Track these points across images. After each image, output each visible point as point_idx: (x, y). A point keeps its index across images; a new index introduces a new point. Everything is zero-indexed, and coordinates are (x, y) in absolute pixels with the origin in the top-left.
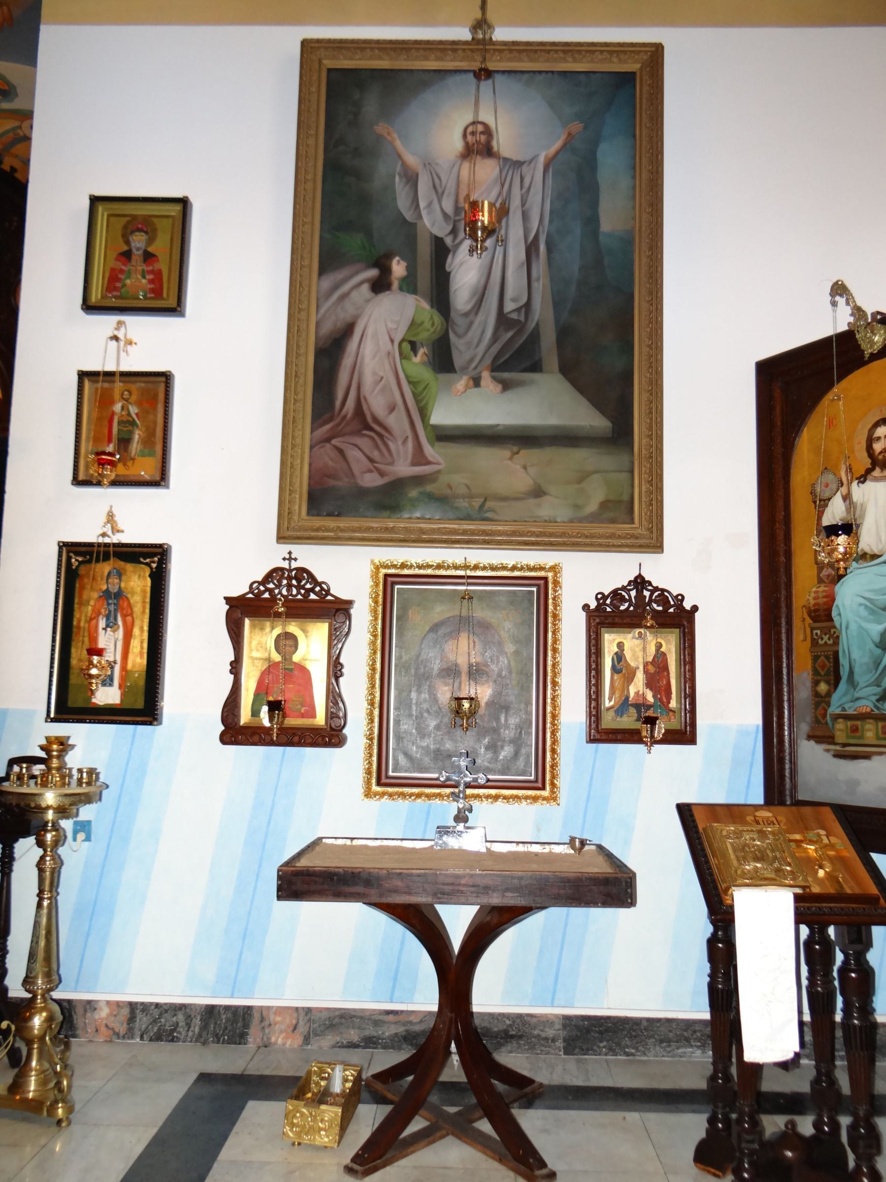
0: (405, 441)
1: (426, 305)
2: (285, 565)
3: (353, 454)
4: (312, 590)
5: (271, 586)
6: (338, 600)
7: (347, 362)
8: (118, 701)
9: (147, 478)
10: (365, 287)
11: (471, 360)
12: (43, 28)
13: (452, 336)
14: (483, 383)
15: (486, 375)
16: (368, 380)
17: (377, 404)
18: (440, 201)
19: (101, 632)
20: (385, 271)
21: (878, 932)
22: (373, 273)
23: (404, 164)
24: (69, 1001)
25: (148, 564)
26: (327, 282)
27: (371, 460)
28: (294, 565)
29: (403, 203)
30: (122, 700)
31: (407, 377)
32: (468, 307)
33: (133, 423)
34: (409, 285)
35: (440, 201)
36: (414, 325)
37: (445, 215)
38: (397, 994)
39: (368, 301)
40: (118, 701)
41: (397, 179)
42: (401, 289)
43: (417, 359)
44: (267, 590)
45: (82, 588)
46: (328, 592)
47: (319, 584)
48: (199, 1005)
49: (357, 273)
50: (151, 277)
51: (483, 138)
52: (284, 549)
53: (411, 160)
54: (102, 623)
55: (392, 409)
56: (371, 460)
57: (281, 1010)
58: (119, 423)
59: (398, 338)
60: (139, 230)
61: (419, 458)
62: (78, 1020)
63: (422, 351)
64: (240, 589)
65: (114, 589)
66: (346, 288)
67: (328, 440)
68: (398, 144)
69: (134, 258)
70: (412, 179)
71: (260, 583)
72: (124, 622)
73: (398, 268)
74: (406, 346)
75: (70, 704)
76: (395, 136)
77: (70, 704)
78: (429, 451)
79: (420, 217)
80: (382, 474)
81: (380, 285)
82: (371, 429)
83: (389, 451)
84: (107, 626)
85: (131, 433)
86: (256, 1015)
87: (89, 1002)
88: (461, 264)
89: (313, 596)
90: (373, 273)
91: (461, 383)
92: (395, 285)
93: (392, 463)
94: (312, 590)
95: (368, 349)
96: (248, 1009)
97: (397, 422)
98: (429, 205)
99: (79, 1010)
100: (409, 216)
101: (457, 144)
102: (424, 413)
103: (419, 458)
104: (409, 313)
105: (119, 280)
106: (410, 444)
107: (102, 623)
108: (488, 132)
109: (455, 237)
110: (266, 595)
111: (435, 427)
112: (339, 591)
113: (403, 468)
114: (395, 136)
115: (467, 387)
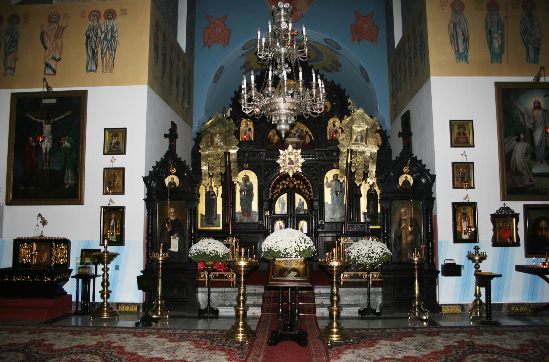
0: (527, 177)
1: (529, 145)
2: (504, 206)
3: (516, 180)
4: (510, 212)
5: (501, 211)
6: (516, 214)
7: (513, 158)
8: (468, 238)
9: (459, 186)
10: (515, 141)
11: (540, 158)
12: (431, 77)
13: (535, 152)
14: (543, 163)
15: (544, 161)
16: (518, 162)
17: (520, 168)
18: (530, 120)
19: (463, 222)
20: (519, 137)
21: (7, 263)
22: (516, 137)
23: (521, 111)
24: (463, 304)
25: (472, 207)
26: (506, 140)
27: (520, 181)
28: (506, 206)
29: (522, 120)
30: (469, 238)
31: (526, 162)
32: (538, 145)
33: (465, 173)
34: (525, 140)
35: (530, 120)
36: (527, 150)
37: (532, 123)
38: (533, 300)
39: (516, 144)
40: (468, 238)
41: (520, 115)
42: (523, 141)
43: (528, 158)
44: (500, 212)
45: (458, 212)
46: (513, 212)
47: (512, 210)
48: (506, 303)
49: (512, 138)
50: (465, 139)
51: (538, 104)
52: (503, 202)
53: (522, 110)
54: (463, 220)
55: (523, 169)
56: (520, 181)
57: (114, 303)
58: (462, 173)
59: (524, 152)
60: (461, 127)
61: (531, 181)
62: (465, 308)
63: (529, 156)
64: (494, 212)
65: (465, 213)
66: (511, 141)
67: (510, 177)
68: (519, 106)
69: (461, 134)
70: (523, 115)
71: (498, 211)
72: (467, 220)
73: (522, 136)
74: (526, 155)
75: (458, 239)
76: (518, 104)
77: (458, 239)
78: (533, 179)
79: (526, 124)
80: (523, 184)
81: (518, 140)
82: (519, 174)
83: (524, 179)
84: (464, 221)
85: (465, 176)
86: (503, 305)
87: (467, 304)
88: (536, 135)
89: (510, 213)
90: (516, 137)
91: (538, 163)
92: (522, 140)
93: (525, 182)
94: (510, 212)
95: (517, 155)
96: (502, 304)
97: (525, 172)
98: (528, 121)
99: (465, 306)
100: (523, 123)
101: (533, 106)
102: (531, 170)
103: (531, 181)
104: (526, 146)
105: (458, 140)
106: (528, 177)
107: (463, 220)
108: (539, 103)
109: (534, 129)
110: (500, 213)
111: (534, 173)
112: (516, 211)
113: (527, 183)
114: (518, 104)
115: (540, 164)
